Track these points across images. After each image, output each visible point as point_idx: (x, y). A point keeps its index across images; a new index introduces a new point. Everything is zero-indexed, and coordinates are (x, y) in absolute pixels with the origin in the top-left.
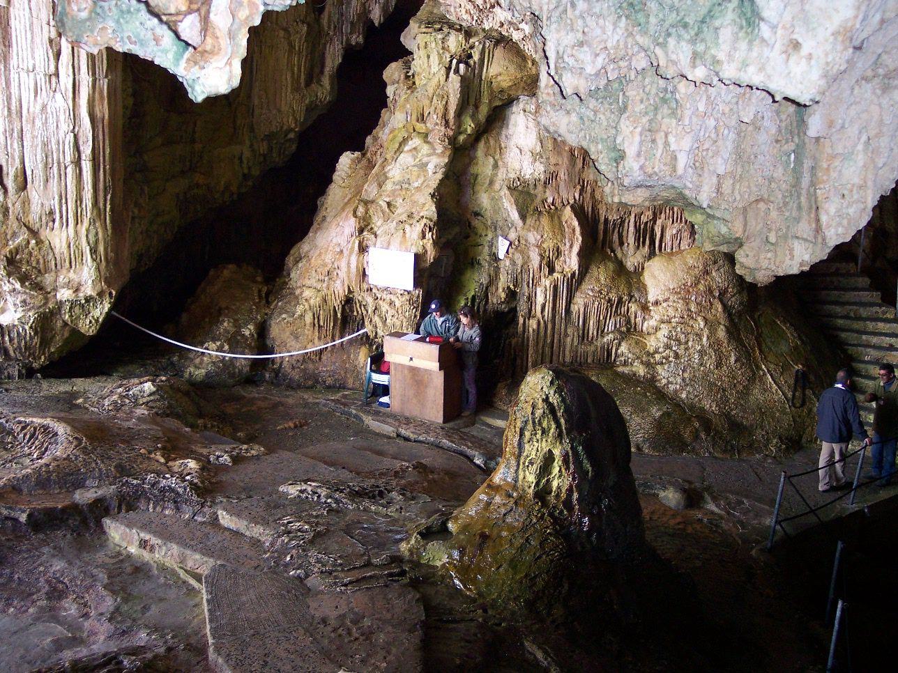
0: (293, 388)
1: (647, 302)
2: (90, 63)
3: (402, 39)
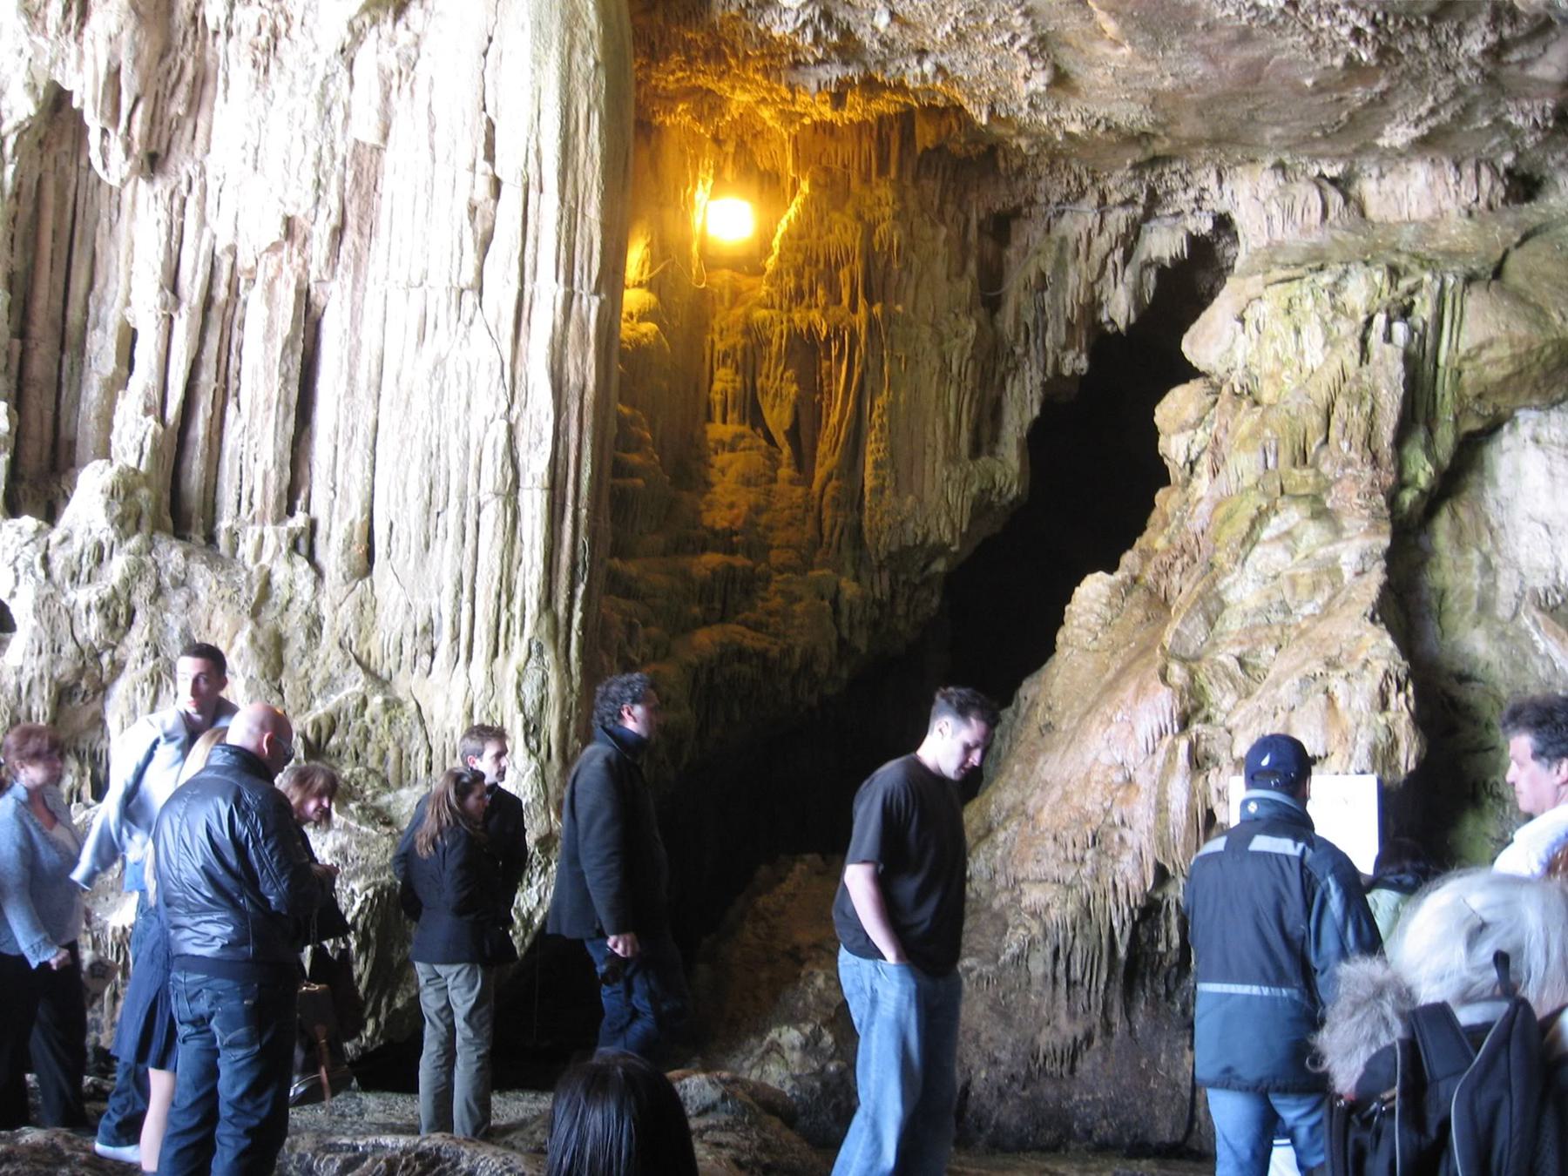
0: (1006, 1150)
2: (563, 255)
3: (1185, 347)
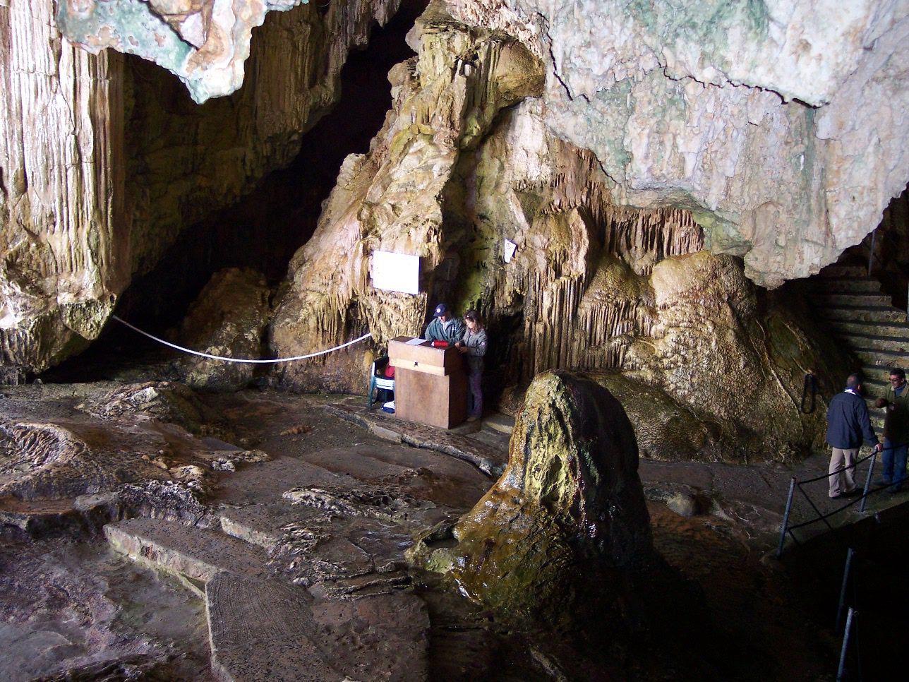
0: (296, 393)
1: (655, 306)
2: (91, 64)
3: (407, 40)
